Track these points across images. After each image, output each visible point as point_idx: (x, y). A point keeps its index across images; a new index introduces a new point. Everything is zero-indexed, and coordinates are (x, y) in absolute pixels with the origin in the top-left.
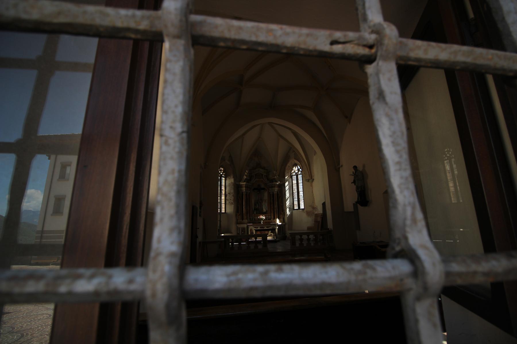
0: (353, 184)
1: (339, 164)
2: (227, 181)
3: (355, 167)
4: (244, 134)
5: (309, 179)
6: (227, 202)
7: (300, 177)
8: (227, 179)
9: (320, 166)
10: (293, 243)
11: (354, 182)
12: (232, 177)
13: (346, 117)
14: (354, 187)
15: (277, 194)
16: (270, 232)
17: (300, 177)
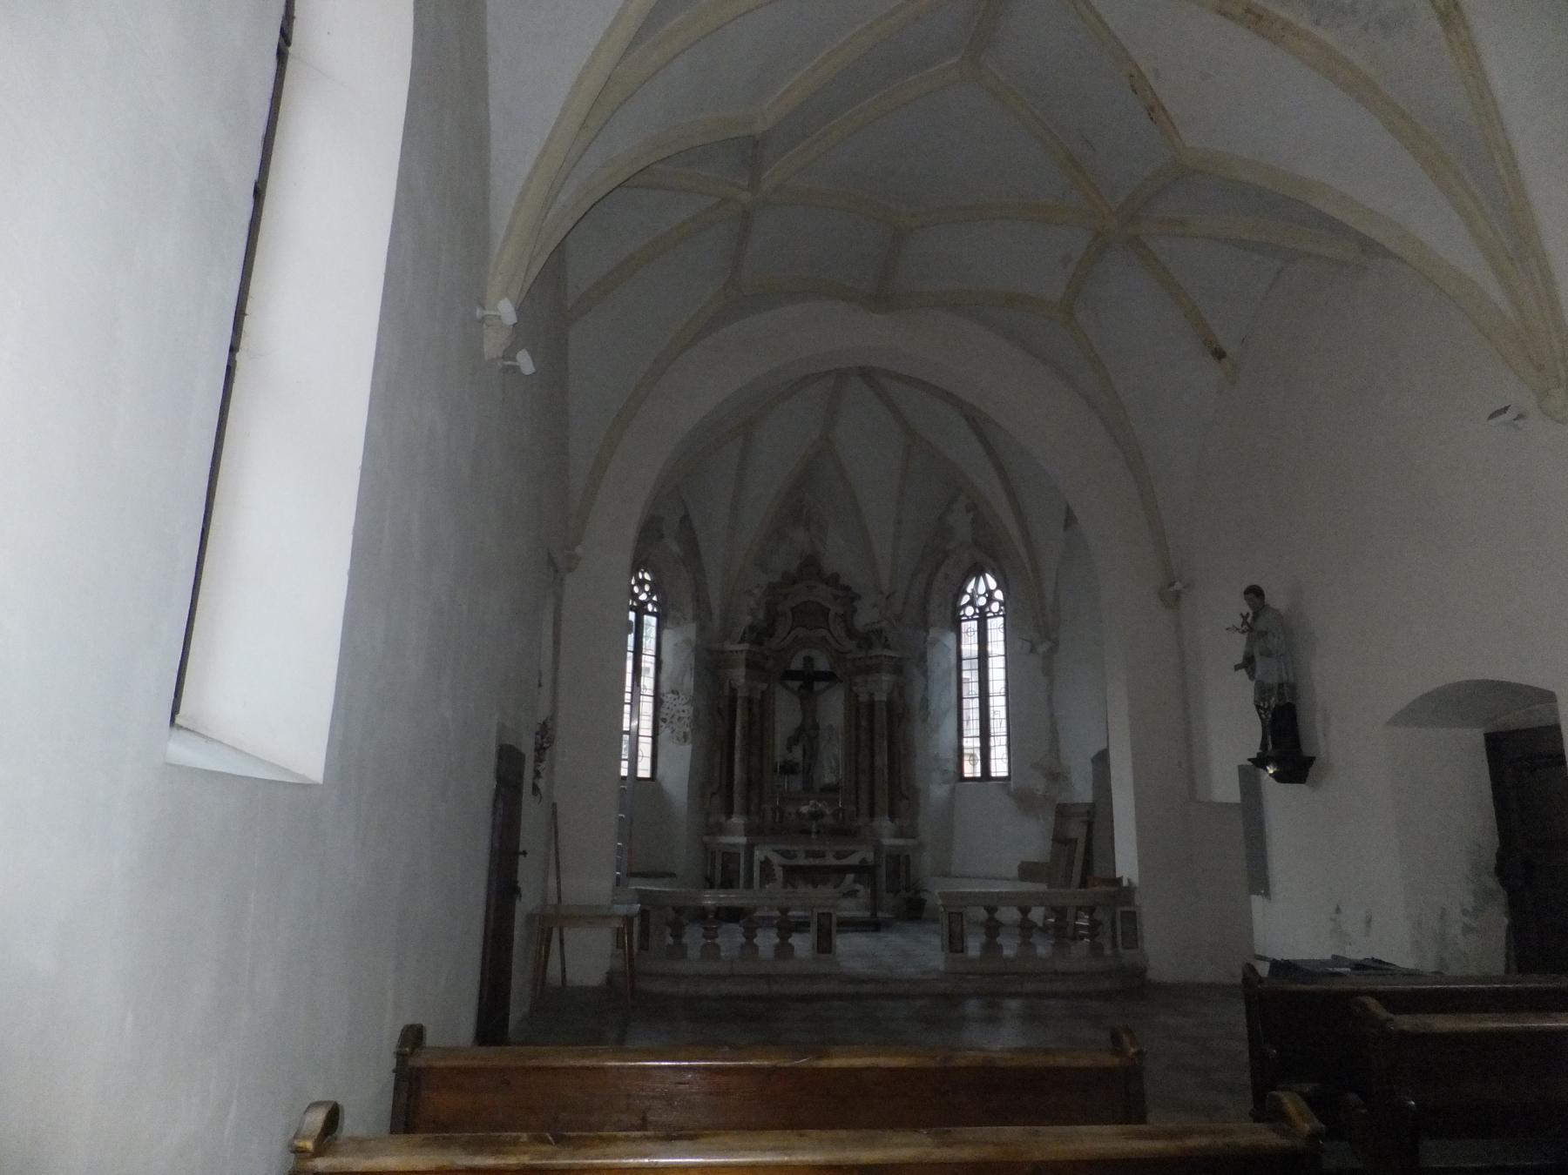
0: (1243, 671)
2: (666, 634)
3: (1255, 593)
7: (996, 626)
10: (955, 943)
11: (1248, 663)
16: (850, 877)
17: (996, 626)
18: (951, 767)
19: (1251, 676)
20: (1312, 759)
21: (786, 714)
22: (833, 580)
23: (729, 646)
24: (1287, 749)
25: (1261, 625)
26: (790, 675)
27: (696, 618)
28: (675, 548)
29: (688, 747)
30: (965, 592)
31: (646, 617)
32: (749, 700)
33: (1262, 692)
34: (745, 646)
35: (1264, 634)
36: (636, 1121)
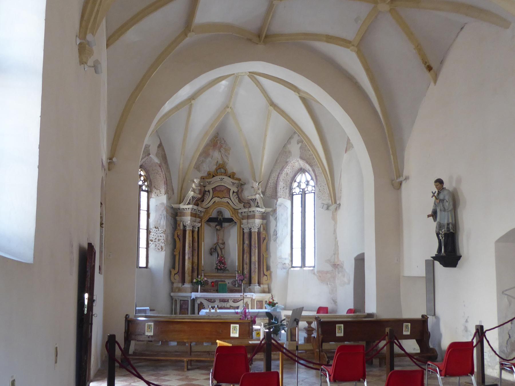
0: (431, 218)
1: (399, 174)
2: (153, 201)
3: (439, 182)
4: (193, 97)
5: (331, 202)
6: (152, 246)
7: (310, 198)
8: (153, 195)
9: (357, 169)
11: (434, 215)
12: (163, 191)
13: (430, 68)
14: (432, 225)
15: (259, 233)
18: (288, 262)
19: (435, 219)
20: (461, 256)
21: (208, 239)
22: (232, 176)
23: (182, 206)
24: (449, 254)
25: (441, 197)
26: (211, 220)
27: (167, 192)
28: (156, 160)
29: (163, 253)
30: (295, 181)
31: (142, 193)
32: (193, 232)
33: (440, 226)
34: (190, 206)
35: (442, 201)
36: (193, 363)
